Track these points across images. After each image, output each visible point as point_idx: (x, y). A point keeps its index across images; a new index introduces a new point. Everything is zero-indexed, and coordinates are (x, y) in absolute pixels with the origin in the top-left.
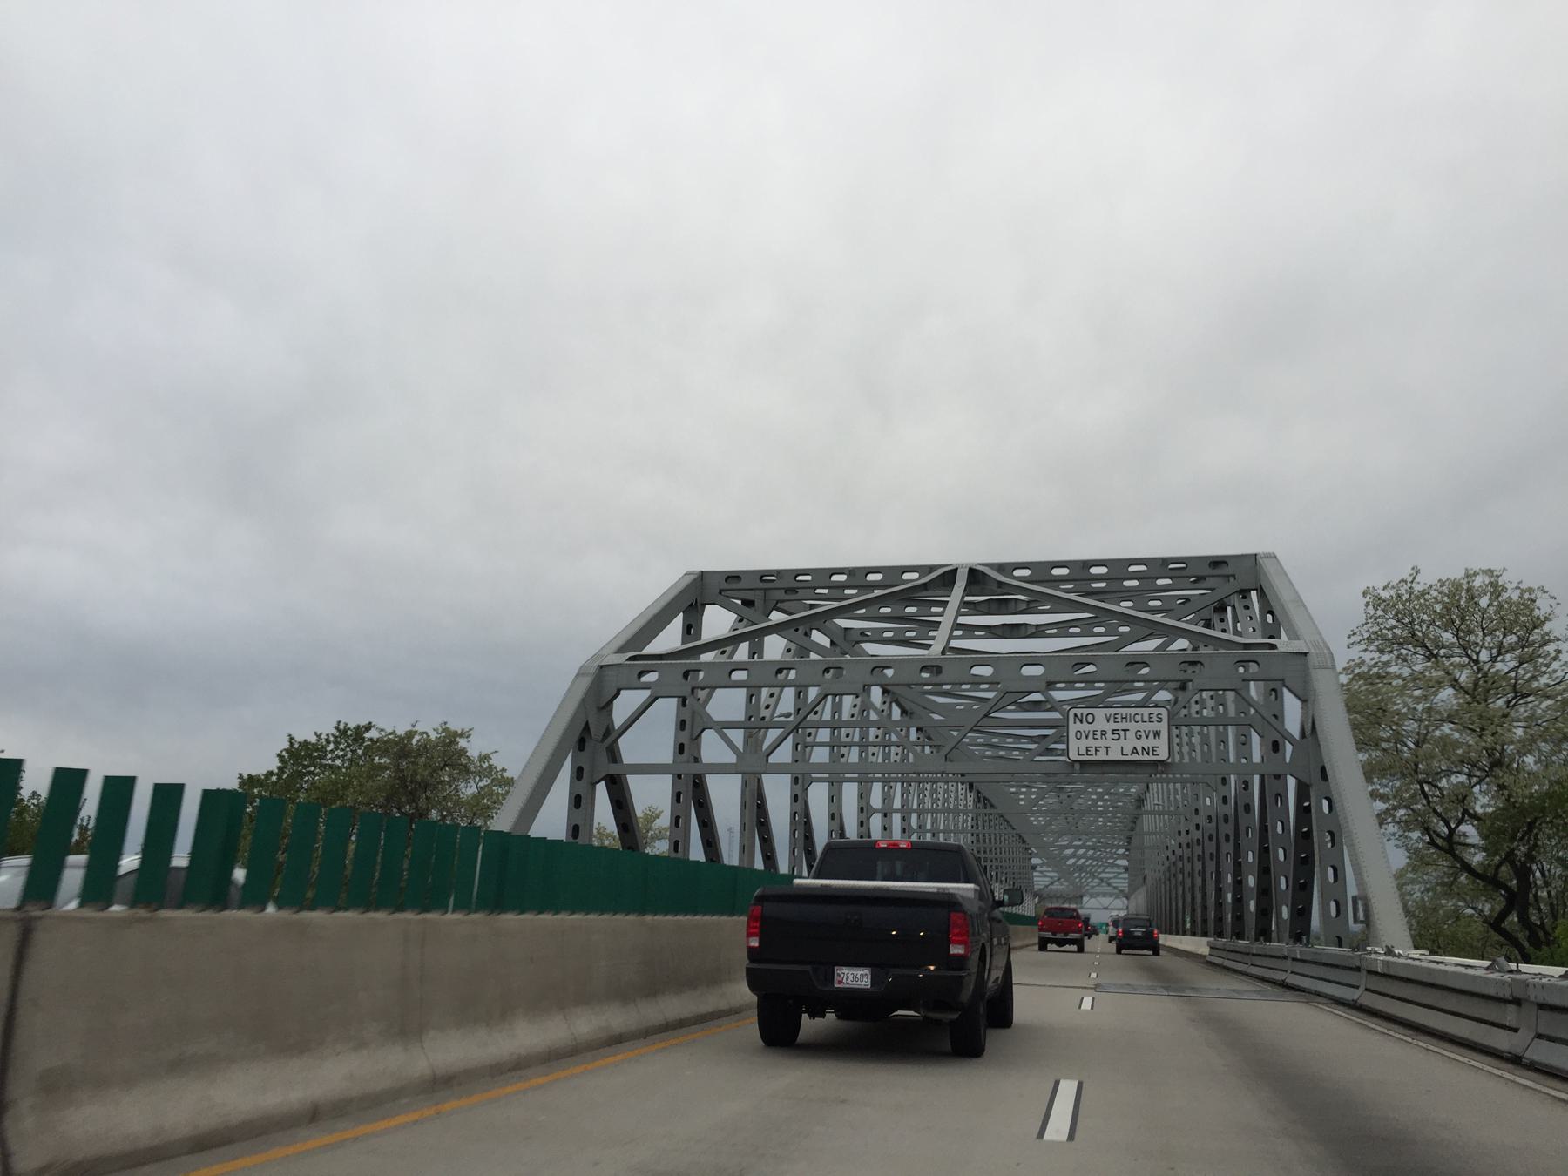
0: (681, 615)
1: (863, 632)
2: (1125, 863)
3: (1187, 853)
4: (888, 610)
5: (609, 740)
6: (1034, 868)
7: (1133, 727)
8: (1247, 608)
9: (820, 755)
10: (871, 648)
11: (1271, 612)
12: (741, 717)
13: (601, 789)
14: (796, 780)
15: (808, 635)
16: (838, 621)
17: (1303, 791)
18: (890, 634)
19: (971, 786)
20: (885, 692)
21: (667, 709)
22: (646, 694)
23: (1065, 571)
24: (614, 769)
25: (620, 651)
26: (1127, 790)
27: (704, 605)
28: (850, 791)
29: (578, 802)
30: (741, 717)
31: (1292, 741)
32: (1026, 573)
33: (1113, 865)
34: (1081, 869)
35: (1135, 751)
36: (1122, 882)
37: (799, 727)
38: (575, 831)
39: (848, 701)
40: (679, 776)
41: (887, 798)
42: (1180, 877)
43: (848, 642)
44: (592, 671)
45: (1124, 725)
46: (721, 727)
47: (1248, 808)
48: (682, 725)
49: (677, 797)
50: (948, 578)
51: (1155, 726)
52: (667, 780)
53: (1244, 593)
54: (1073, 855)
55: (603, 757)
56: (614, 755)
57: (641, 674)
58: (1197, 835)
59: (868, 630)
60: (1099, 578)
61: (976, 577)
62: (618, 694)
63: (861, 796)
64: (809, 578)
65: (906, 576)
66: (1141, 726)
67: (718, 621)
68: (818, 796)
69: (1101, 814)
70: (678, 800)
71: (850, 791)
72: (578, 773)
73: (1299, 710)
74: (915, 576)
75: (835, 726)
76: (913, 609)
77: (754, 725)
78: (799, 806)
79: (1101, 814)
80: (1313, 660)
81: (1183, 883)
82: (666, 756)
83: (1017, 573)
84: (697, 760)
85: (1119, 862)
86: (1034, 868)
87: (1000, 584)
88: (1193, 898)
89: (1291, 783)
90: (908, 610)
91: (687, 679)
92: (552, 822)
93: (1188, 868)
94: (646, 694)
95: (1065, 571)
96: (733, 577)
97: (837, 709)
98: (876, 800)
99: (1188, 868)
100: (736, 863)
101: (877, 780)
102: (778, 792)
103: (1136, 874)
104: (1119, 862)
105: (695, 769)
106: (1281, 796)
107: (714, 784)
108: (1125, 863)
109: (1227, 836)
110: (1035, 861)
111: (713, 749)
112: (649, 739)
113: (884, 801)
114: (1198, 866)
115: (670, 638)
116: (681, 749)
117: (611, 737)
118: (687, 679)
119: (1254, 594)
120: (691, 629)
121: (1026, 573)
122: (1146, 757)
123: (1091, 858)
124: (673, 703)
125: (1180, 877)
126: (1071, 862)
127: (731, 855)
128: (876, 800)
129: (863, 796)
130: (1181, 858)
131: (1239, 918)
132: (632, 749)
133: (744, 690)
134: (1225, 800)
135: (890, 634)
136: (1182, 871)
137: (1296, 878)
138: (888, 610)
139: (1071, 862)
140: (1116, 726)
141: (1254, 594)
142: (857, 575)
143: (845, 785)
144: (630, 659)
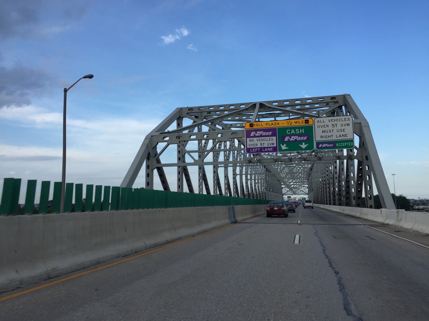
0: (176, 121)
1: (231, 125)
2: (307, 186)
3: (325, 183)
4: (238, 118)
5: (156, 157)
6: (282, 188)
7: (339, 123)
8: (341, 112)
9: (221, 158)
10: (233, 129)
11: (349, 112)
12: (197, 150)
13: (155, 172)
14: (214, 167)
15: (215, 126)
16: (223, 122)
17: (360, 163)
18: (239, 125)
19: (265, 167)
20: (239, 141)
21: (174, 148)
22: (166, 143)
23: (288, 103)
24: (159, 165)
25: (157, 132)
26: (308, 166)
27: (182, 118)
28: (230, 169)
29: (149, 175)
30: (197, 150)
31: (356, 148)
32: (276, 104)
33: (304, 187)
34: (296, 187)
35: (340, 136)
36: (307, 190)
37: (216, 152)
38: (148, 184)
39: (228, 143)
40: (179, 167)
41: (241, 171)
42: (323, 189)
43: (225, 127)
44: (149, 137)
45: (336, 122)
46: (189, 152)
47: (336, 173)
48: (179, 152)
49: (179, 173)
50: (254, 106)
51: (347, 122)
52: (176, 168)
53: (340, 107)
54: (293, 184)
55: (155, 162)
56: (158, 161)
57: (164, 138)
58: (327, 177)
59: (233, 124)
60: (298, 105)
61: (262, 106)
62: (158, 144)
63: (233, 171)
64: (213, 108)
65: (241, 106)
66: (341, 122)
67: (187, 122)
68: (221, 171)
69: (301, 173)
70: (179, 174)
71: (230, 169)
72: (148, 167)
73: (358, 140)
74: (244, 106)
75: (225, 151)
76: (245, 117)
77: (202, 152)
78: (235, 183)
79: (301, 173)
80: (363, 124)
81: (323, 191)
82: (175, 161)
83: (274, 104)
84: (184, 162)
85: (305, 186)
86: (282, 188)
87: (269, 107)
88: (326, 194)
89: (356, 161)
90: (244, 117)
91: (180, 139)
92: (140, 182)
93: (325, 186)
94: (166, 143)
95: (288, 103)
96: (191, 109)
97: (225, 146)
98: (238, 171)
99: (325, 186)
100: (176, 191)
101: (238, 166)
102: (209, 170)
103: (310, 189)
104: (305, 186)
105: (184, 164)
106: (343, 170)
107: (189, 168)
108: (307, 186)
109: (336, 178)
110: (283, 186)
111: (188, 159)
112: (169, 155)
113: (240, 172)
114: (328, 186)
115: (173, 127)
116: (179, 159)
117: (157, 157)
118: (180, 139)
119: (343, 107)
120: (179, 125)
121: (276, 104)
122: (344, 138)
123: (298, 185)
124: (175, 146)
125: (323, 189)
126: (292, 186)
127: (173, 187)
128: (238, 171)
129: (234, 171)
130: (323, 184)
131: (334, 200)
132: (163, 159)
133: (197, 141)
134: (336, 167)
135: (239, 125)
136: (323, 187)
137: (357, 189)
138: (238, 118)
139: (292, 186)
140: (333, 123)
141: (343, 107)
142: (227, 107)
143: (223, 160)
144: (160, 134)
